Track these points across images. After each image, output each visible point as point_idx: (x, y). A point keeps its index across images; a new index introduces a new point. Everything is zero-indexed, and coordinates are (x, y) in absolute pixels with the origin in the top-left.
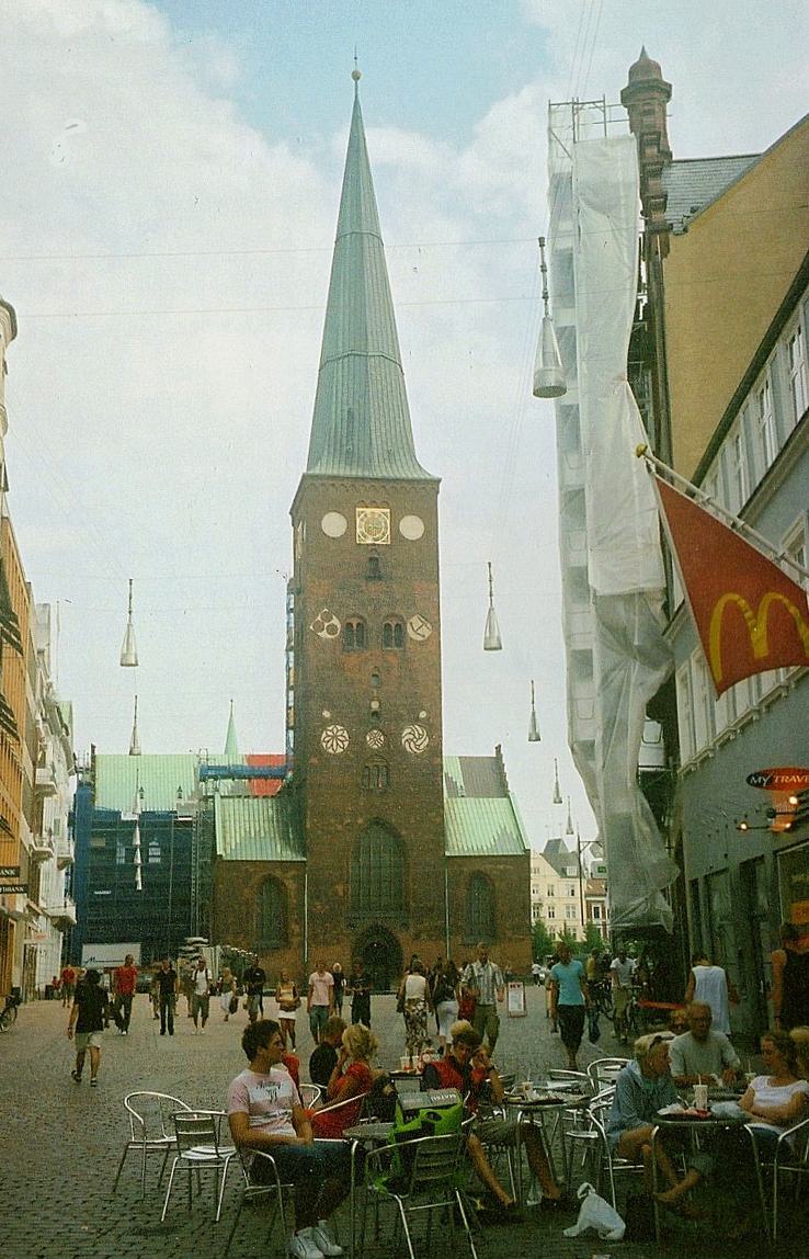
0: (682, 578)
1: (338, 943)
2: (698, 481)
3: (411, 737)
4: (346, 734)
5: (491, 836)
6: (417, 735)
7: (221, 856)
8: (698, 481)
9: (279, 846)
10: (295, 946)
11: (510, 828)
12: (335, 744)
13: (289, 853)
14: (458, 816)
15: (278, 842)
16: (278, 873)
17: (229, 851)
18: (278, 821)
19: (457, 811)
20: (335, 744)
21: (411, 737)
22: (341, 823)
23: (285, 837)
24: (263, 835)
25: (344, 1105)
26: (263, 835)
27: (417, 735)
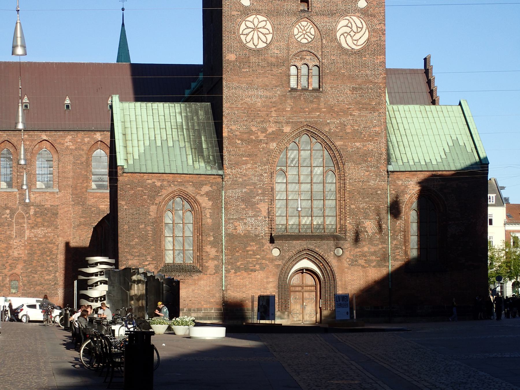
0: (440, 173)
1: (262, 268)
2: (158, 105)
3: (348, 30)
4: (269, 26)
5: (441, 149)
6: (355, 29)
7: (122, 166)
8: (158, 105)
9: (190, 157)
10: (211, 270)
11: (465, 139)
12: (261, 36)
13: (202, 164)
14: (401, 126)
15: (189, 152)
16: (190, 190)
17: (131, 162)
18: (188, 129)
19: (399, 120)
20: (261, 36)
21: (348, 30)
22: (264, 130)
23: (198, 150)
24: (170, 144)
25: (360, 326)
26: (170, 144)
27: (355, 29)
